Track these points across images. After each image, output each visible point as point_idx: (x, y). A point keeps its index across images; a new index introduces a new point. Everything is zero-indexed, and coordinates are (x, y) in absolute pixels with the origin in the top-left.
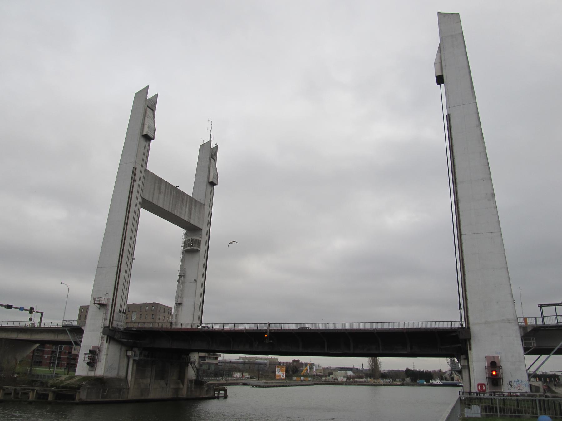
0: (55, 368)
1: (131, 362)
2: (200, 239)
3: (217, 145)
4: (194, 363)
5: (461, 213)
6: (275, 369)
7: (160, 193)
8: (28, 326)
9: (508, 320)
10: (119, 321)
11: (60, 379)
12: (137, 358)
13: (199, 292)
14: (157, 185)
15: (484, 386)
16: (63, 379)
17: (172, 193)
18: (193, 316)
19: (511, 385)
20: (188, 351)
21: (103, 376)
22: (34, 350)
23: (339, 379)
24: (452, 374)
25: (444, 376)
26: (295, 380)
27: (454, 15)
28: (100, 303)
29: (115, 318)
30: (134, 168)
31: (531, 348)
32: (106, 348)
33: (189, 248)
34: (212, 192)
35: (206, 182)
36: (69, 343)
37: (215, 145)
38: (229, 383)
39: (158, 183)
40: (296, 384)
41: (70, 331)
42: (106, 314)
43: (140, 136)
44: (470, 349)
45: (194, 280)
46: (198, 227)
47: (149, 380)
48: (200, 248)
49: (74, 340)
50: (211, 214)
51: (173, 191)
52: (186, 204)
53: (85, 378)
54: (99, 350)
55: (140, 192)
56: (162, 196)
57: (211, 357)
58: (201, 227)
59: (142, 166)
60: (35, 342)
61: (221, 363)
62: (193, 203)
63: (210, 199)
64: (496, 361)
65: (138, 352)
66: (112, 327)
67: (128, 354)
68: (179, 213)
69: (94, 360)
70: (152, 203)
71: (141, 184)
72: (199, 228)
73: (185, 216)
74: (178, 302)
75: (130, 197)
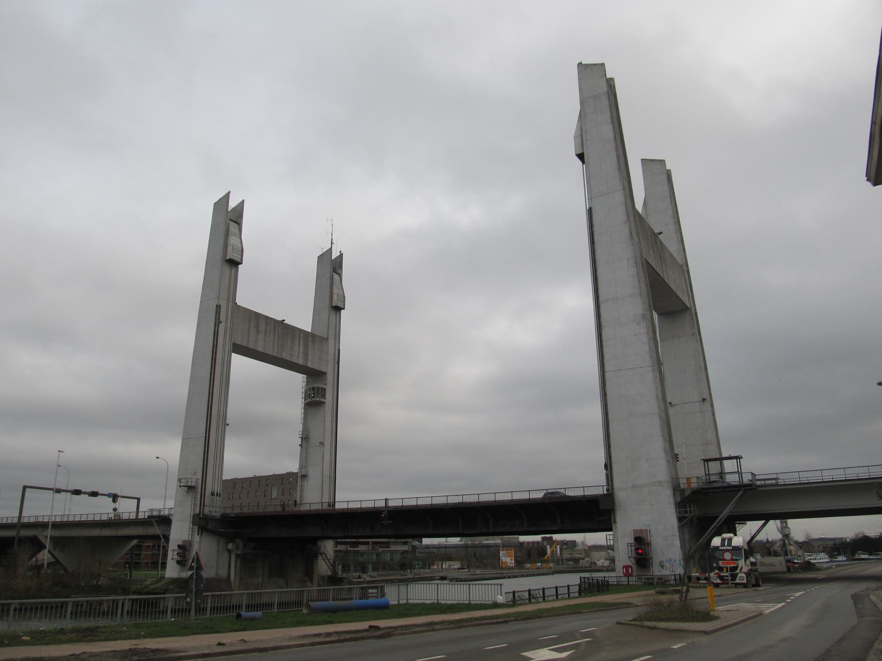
2: (324, 387)
4: (324, 554)
5: (604, 343)
6: (500, 554)
7: (258, 333)
8: (113, 519)
9: (660, 482)
10: (212, 506)
11: (145, 583)
12: (239, 552)
13: (327, 458)
15: (630, 569)
16: (149, 583)
17: (277, 330)
19: (662, 567)
20: (315, 540)
22: (133, 546)
23: (598, 563)
24: (784, 545)
25: (772, 549)
26: (529, 568)
27: (597, 65)
28: (190, 484)
30: (217, 306)
31: (686, 517)
32: (198, 542)
33: (309, 400)
34: (338, 319)
35: (328, 307)
36: (156, 537)
38: (417, 578)
40: (484, 576)
41: (157, 522)
42: (195, 498)
43: (222, 261)
44: (615, 522)
45: (320, 443)
49: (163, 534)
50: (339, 350)
52: (299, 342)
53: (174, 581)
55: (228, 336)
56: (261, 337)
57: (397, 542)
58: (324, 370)
59: (228, 300)
60: (131, 538)
61: (433, 548)
62: (310, 339)
63: (336, 330)
64: (644, 535)
65: (241, 544)
66: (204, 515)
67: (228, 548)
68: (288, 356)
69: (184, 557)
70: (248, 348)
71: (229, 325)
72: (321, 371)
74: (303, 474)
75: (215, 344)
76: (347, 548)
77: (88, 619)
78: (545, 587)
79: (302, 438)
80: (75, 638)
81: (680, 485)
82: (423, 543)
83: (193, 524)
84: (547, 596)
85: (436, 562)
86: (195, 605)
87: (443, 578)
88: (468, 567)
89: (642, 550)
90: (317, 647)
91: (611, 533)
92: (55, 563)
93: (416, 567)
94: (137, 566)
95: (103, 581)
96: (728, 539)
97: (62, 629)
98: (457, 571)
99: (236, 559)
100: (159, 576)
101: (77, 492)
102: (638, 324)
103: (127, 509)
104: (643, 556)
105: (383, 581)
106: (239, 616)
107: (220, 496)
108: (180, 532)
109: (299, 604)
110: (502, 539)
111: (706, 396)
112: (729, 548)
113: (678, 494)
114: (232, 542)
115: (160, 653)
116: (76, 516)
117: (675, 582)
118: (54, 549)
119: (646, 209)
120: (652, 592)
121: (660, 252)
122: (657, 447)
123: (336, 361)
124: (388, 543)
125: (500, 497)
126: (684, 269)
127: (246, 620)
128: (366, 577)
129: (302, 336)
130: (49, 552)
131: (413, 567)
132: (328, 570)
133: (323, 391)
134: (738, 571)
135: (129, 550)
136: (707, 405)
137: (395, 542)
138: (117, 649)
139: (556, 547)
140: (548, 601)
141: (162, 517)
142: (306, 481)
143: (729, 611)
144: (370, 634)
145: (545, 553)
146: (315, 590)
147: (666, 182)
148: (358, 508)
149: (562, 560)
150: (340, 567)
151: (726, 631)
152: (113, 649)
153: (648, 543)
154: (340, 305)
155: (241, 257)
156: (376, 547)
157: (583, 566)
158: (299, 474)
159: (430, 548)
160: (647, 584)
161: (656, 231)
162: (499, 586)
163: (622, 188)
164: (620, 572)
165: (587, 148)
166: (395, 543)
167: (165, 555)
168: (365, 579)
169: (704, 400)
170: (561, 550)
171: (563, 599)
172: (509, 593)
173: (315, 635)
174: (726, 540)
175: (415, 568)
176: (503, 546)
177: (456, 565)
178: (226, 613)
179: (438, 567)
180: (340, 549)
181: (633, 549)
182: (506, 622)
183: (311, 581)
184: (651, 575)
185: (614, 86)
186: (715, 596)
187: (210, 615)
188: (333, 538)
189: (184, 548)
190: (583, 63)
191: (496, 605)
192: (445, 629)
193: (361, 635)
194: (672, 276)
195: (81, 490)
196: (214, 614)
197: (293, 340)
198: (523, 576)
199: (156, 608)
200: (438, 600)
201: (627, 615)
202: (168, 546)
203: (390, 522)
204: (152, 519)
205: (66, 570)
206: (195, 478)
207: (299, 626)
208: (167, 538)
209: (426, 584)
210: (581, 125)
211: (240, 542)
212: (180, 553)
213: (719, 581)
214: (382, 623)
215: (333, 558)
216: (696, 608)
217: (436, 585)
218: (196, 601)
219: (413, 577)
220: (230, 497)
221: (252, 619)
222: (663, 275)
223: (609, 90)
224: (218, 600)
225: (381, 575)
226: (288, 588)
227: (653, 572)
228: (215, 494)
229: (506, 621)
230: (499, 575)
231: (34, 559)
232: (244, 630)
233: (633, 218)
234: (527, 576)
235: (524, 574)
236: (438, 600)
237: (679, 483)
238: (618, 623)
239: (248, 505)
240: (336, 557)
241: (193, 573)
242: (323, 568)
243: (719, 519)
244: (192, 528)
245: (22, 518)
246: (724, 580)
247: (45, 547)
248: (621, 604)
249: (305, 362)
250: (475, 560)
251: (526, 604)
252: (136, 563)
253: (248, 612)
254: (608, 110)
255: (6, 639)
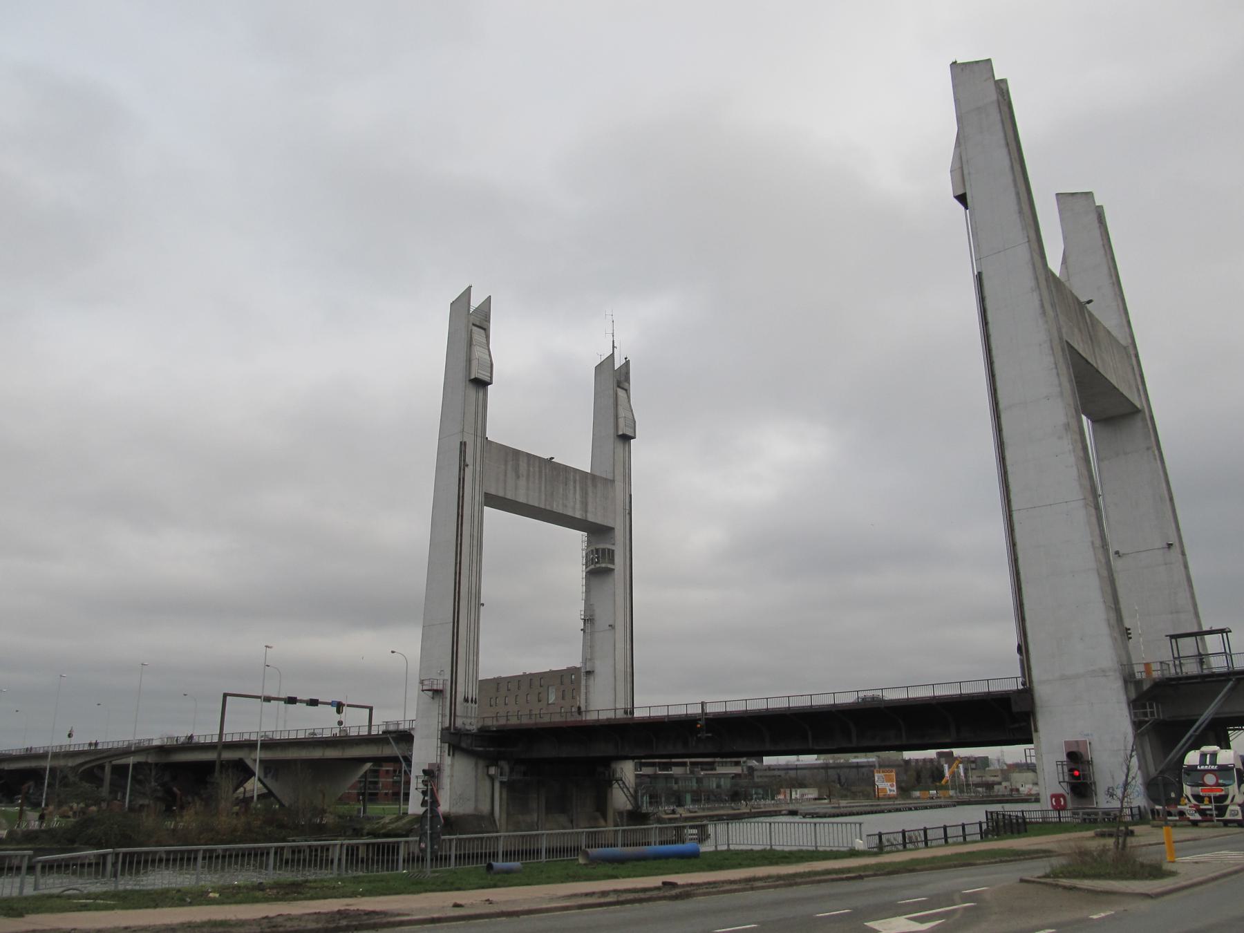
0: (402, 804)
1: (497, 785)
3: (629, 361)
4: (622, 780)
5: (1009, 468)
6: (874, 777)
7: (518, 477)
8: (338, 735)
9: (1103, 671)
10: (466, 717)
11: (382, 821)
12: (505, 779)
13: (621, 645)
14: (510, 464)
15: (1062, 799)
16: (387, 821)
18: (613, 692)
19: (1112, 795)
20: (607, 761)
21: (449, 812)
22: (366, 772)
23: (1021, 789)
26: (918, 798)
27: (980, 63)
28: (435, 687)
29: (458, 713)
30: (461, 443)
31: (1147, 722)
32: (448, 766)
33: (592, 567)
36: (394, 760)
37: (624, 361)
39: (513, 460)
42: (443, 706)
44: (1036, 731)
45: (610, 626)
46: (605, 524)
47: (535, 816)
48: (613, 563)
50: (631, 495)
51: (543, 468)
54: (439, 770)
55: (477, 482)
57: (726, 762)
58: (610, 525)
60: (363, 760)
61: (779, 769)
62: (589, 482)
64: (1082, 750)
65: (506, 768)
66: (455, 728)
71: (478, 469)
73: (574, 508)
76: (656, 770)
77: (278, 872)
78: (927, 827)
79: (585, 620)
80: (274, 896)
81: (1134, 674)
82: (765, 763)
83: (441, 742)
84: (931, 840)
85: (782, 790)
86: (431, 853)
87: (793, 813)
88: (829, 797)
89: (1079, 771)
90: (585, 910)
91: (1031, 746)
92: (268, 795)
93: (754, 796)
94: (373, 797)
95: (328, 819)
96: (1211, 754)
97: (261, 883)
98: (813, 802)
99: (501, 788)
100: (402, 812)
101: (292, 700)
102: (1060, 438)
103: (356, 723)
104: (1082, 781)
105: (706, 817)
106: (490, 867)
107: (476, 703)
108: (425, 752)
109: (576, 850)
110: (878, 757)
111: (1173, 539)
112: (1213, 767)
113: (1132, 688)
114: (495, 766)
115: (377, 917)
116: (361, 728)
117: (1132, 819)
118: (266, 776)
119: (1067, 268)
120: (1091, 833)
121: (1090, 328)
122: (1097, 617)
123: (627, 511)
124: (712, 763)
125: (968, 689)
126: (1130, 353)
127: (498, 872)
128: (682, 812)
129: (578, 478)
130: (259, 780)
131: (749, 798)
132: (628, 802)
133: (611, 554)
134: (1228, 802)
135: (362, 777)
136: (1176, 550)
137: (722, 762)
138: (322, 911)
139: (958, 767)
140: (932, 847)
141: (401, 732)
142: (592, 678)
143: (1196, 863)
144: (661, 893)
145: (942, 776)
146: (610, 831)
147: (1096, 224)
148: (665, 716)
149: (968, 785)
150: (646, 799)
151: (1186, 892)
152: (318, 911)
153: (1088, 762)
154: (629, 433)
155: (489, 375)
156: (696, 769)
157: (999, 793)
158: (583, 670)
159: (774, 769)
160: (1087, 821)
161: (1083, 299)
162: (858, 826)
163: (1027, 240)
164: (1046, 803)
165: (971, 185)
166: (723, 764)
167: (408, 783)
168: (681, 815)
169: (1170, 545)
170: (966, 770)
171: (955, 844)
172: (872, 835)
173: (587, 895)
174: (1208, 756)
175: (752, 799)
176: (880, 766)
177: (812, 793)
178: (477, 863)
179: (785, 796)
180: (646, 773)
181: (1066, 769)
182: (861, 877)
183: (605, 818)
184: (1095, 808)
185: (1008, 91)
186: (1174, 842)
187: (456, 865)
188: (633, 758)
189: (431, 774)
190: (958, 62)
191: (853, 853)
192: (769, 887)
193: (648, 894)
194: (1111, 364)
195: (318, 700)
196: (460, 865)
197: (566, 485)
198: (910, 809)
199: (393, 855)
200: (771, 846)
201: (1037, 869)
202: (410, 771)
203: (710, 735)
204: (388, 735)
205: (282, 805)
206: (442, 679)
207: (570, 882)
208: (408, 761)
209: (754, 823)
210: (960, 153)
211: (505, 765)
212: (426, 781)
213: (1197, 817)
214: (680, 879)
215: (634, 786)
216: (1141, 859)
217: (768, 825)
218: (432, 848)
219: (748, 811)
220: (493, 703)
221: (508, 872)
222: (1096, 362)
223: (1000, 98)
224: (477, 845)
225: (704, 809)
226: (573, 829)
227: (1097, 803)
228: (470, 699)
229: (860, 875)
230: (874, 808)
231: (241, 789)
232: (495, 886)
233: (1045, 283)
234: (916, 809)
235: (911, 806)
236: (771, 846)
237: (1133, 670)
238: (1022, 881)
239: (516, 714)
240: (638, 785)
241: (427, 810)
242: (620, 799)
243: (1197, 724)
244: (441, 747)
245: (224, 736)
246: (1206, 815)
247: (254, 774)
248: (1037, 852)
249: (584, 515)
250: (838, 786)
251: (898, 851)
252: (371, 794)
253: (506, 861)
254: (999, 126)
255: (190, 896)
